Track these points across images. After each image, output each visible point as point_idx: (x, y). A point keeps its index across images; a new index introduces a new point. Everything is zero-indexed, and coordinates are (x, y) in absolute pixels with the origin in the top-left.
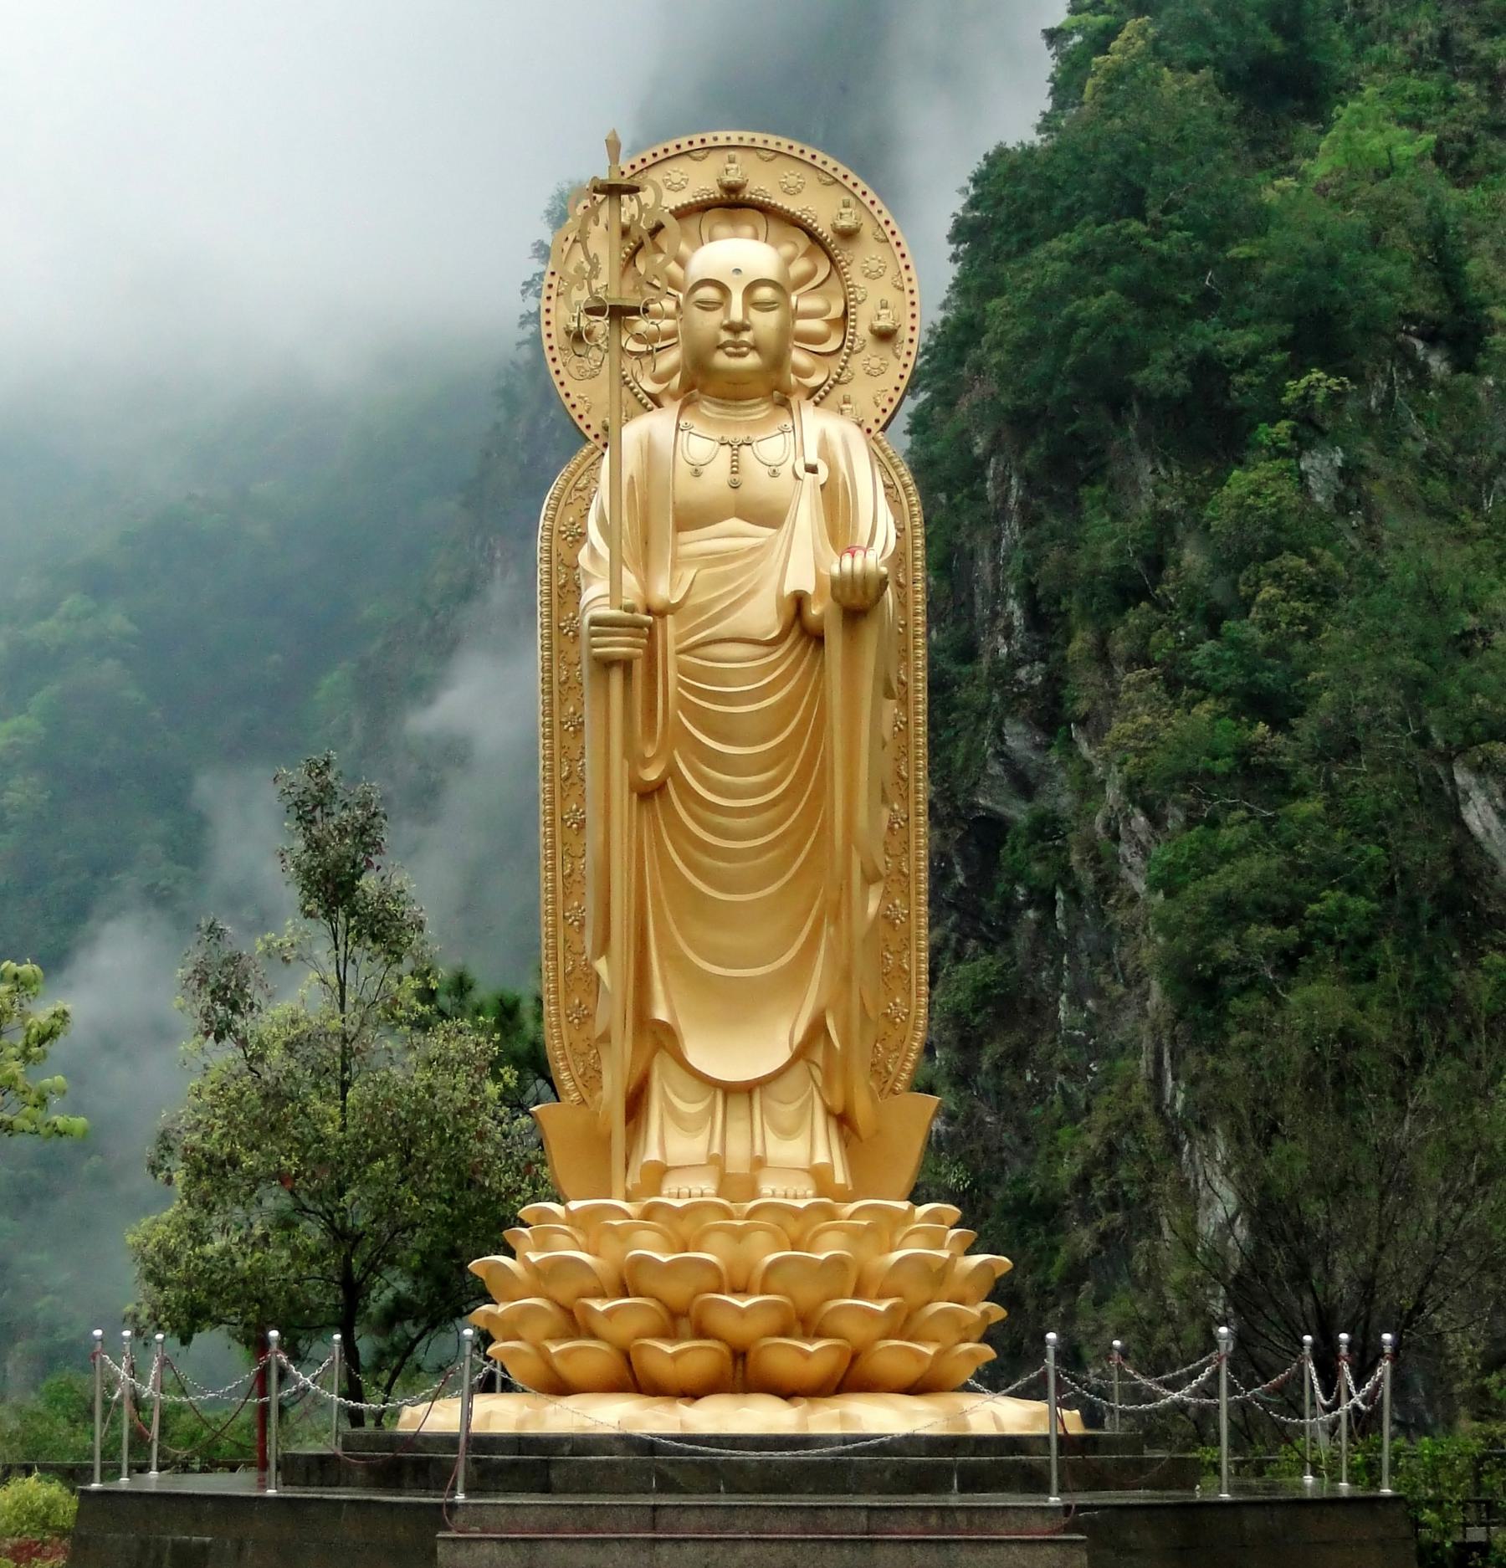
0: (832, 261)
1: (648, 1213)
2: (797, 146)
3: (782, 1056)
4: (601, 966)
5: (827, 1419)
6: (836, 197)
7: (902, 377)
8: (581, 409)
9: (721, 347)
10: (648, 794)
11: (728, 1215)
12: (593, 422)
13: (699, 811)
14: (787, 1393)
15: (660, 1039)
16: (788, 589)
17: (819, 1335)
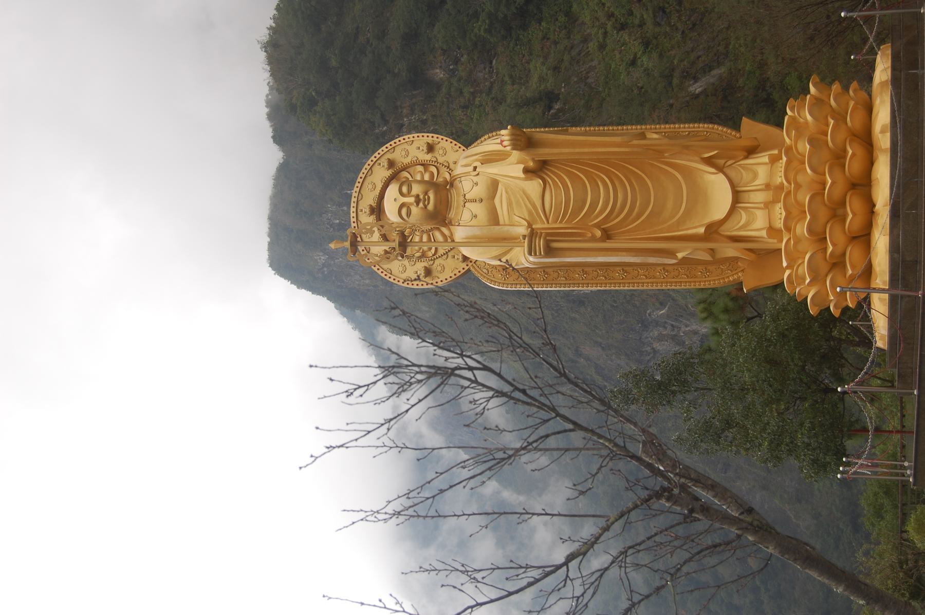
1: (788, 229)
2: (357, 184)
3: (721, 176)
4: (680, 255)
5: (883, 140)
6: (376, 168)
8: (456, 272)
9: (426, 207)
10: (607, 235)
11: (788, 193)
12: (462, 267)
13: (615, 214)
14: (870, 162)
15: (713, 230)
16: (522, 175)
17: (845, 151)
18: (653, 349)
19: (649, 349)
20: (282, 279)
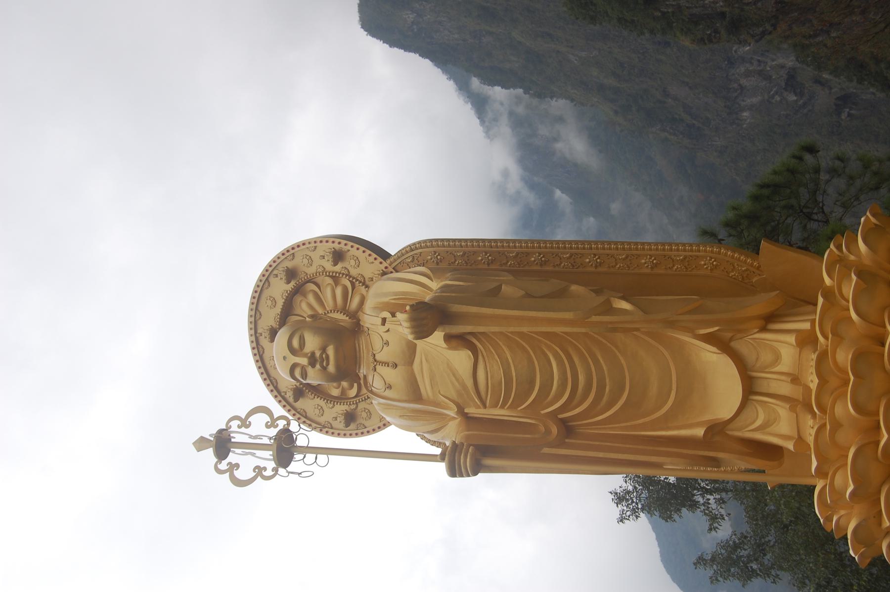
0: (308, 282)
7: (358, 249)
9: (324, 368)
13: (576, 402)
18: (740, 85)
19: (735, 86)
20: (375, 39)
